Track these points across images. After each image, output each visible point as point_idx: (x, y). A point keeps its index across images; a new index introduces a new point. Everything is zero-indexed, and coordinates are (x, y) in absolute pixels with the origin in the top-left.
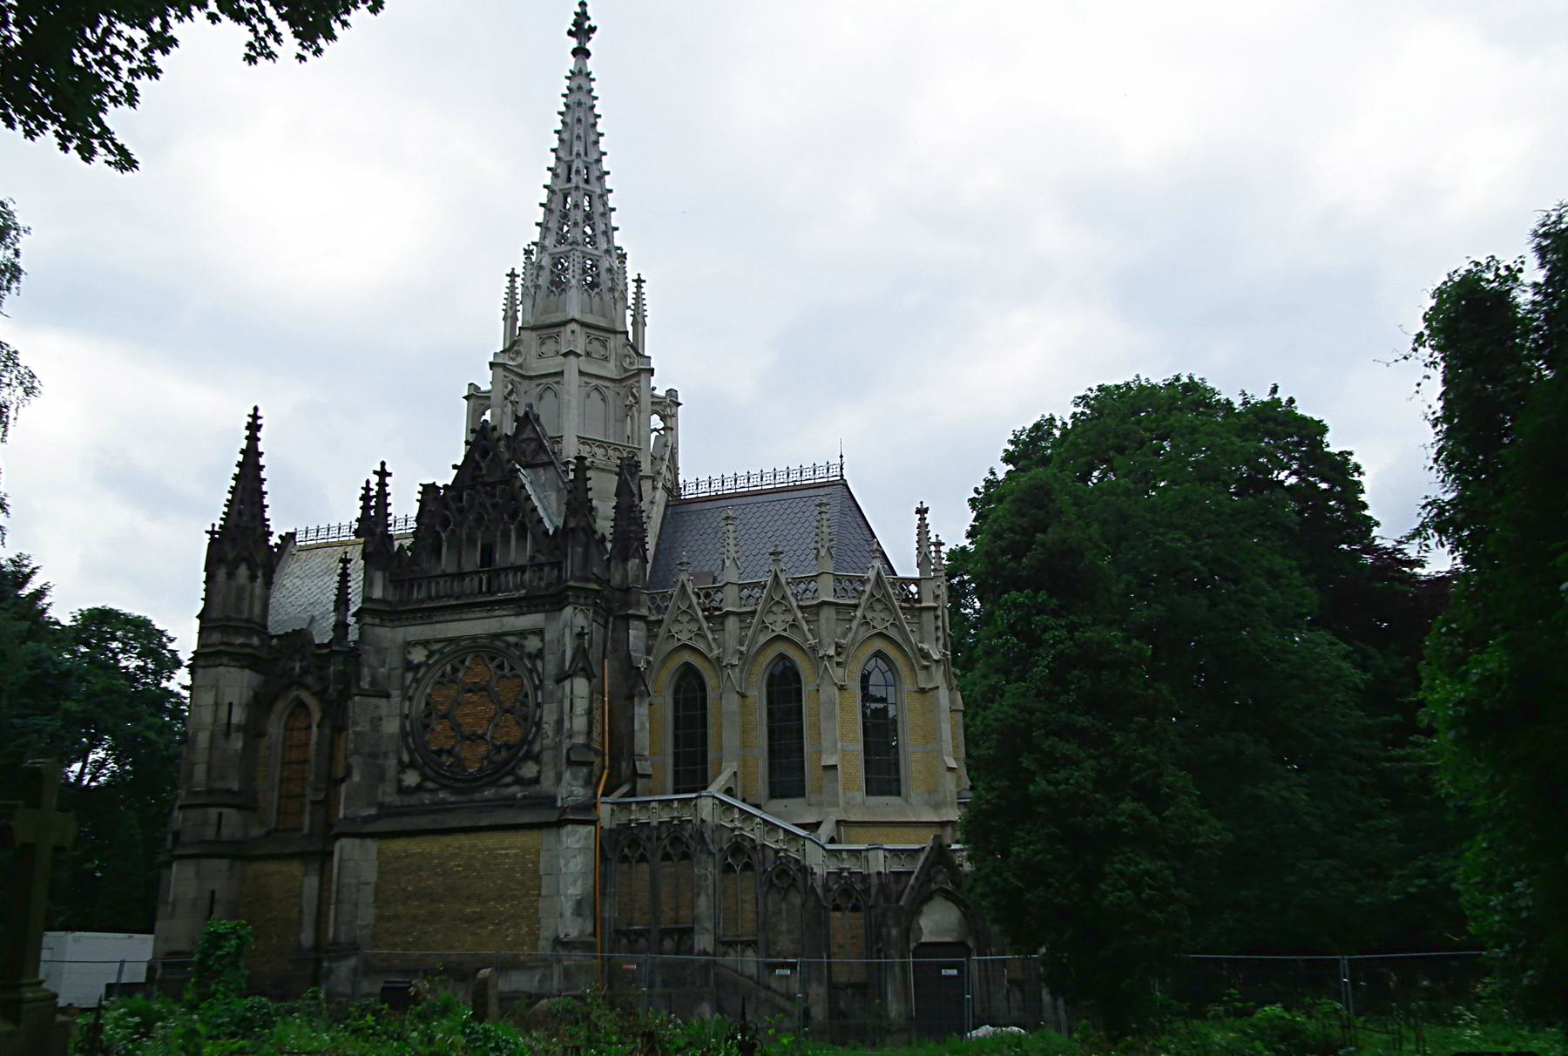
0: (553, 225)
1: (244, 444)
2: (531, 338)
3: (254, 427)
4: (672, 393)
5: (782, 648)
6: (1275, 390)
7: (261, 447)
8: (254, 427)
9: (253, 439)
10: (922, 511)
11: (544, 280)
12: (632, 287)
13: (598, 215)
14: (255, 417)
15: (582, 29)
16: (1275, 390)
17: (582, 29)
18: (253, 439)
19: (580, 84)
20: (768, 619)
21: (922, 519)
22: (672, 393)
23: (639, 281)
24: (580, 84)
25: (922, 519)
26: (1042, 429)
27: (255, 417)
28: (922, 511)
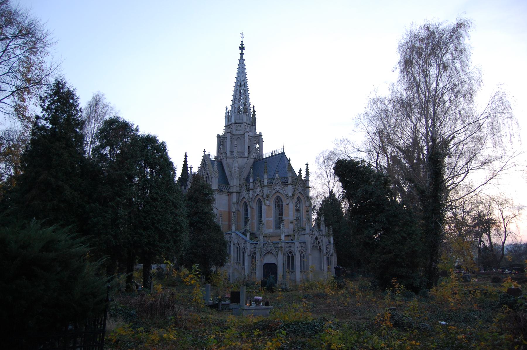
0: (237, 97)
1: (184, 160)
2: (234, 126)
3: (186, 156)
4: (260, 133)
5: (278, 194)
6: (205, 152)
7: (187, 160)
8: (186, 156)
9: (186, 159)
10: (307, 164)
11: (236, 111)
12: (252, 109)
13: (246, 92)
14: (186, 154)
15: (242, 48)
16: (205, 152)
17: (242, 48)
18: (186, 159)
19: (242, 60)
20: (275, 187)
21: (307, 166)
22: (260, 133)
23: (254, 107)
24: (242, 60)
25: (307, 166)
26: (125, 126)
27: (186, 154)
28: (307, 164)
